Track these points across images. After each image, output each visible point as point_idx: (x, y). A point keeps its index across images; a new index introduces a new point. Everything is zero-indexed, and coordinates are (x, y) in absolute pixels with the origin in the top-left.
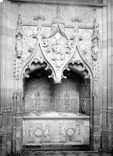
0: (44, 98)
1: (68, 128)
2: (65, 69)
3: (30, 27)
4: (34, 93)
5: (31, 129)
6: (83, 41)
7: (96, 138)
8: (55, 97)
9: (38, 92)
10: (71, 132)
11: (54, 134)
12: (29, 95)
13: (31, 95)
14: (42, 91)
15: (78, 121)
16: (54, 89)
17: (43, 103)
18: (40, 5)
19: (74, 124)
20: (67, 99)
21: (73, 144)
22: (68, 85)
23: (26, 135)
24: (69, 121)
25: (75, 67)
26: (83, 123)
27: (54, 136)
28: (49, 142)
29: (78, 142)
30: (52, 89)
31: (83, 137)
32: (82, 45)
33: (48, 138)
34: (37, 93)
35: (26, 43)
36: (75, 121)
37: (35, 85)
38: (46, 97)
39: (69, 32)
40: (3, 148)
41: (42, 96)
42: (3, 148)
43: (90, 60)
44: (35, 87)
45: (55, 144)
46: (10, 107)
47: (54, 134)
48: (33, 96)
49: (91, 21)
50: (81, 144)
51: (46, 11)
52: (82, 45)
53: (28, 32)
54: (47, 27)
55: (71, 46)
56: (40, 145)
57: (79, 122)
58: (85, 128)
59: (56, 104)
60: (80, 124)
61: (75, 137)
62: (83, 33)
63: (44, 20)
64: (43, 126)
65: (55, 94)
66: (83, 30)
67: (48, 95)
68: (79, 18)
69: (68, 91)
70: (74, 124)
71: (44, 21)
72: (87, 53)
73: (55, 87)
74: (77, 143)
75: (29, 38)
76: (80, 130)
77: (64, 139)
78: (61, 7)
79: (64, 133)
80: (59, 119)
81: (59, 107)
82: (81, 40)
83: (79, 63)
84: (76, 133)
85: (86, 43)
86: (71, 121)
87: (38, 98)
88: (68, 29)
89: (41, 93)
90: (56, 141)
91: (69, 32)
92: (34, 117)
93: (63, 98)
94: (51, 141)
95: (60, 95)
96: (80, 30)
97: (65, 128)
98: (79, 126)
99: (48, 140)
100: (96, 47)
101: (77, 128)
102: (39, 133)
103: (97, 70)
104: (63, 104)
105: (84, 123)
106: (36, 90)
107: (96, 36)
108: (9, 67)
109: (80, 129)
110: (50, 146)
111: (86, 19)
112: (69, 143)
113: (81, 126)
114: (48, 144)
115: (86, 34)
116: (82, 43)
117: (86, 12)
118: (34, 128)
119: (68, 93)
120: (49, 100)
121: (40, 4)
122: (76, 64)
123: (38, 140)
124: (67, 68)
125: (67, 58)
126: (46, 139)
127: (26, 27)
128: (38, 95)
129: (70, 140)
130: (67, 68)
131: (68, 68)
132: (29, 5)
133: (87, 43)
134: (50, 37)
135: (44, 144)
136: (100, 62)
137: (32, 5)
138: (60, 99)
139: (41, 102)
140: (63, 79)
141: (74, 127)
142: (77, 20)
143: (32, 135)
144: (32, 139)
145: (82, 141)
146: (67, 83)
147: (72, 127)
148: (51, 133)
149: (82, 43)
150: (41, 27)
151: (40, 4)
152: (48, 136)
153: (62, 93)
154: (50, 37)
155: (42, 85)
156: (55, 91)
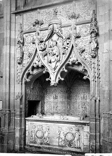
0: (62, 100)
1: (67, 132)
2: (61, 70)
3: (31, 33)
4: (52, 96)
5: (33, 130)
6: (81, 38)
7: (93, 147)
8: (72, 100)
9: (56, 95)
10: (69, 137)
11: (53, 137)
12: (48, 98)
13: (50, 98)
14: (59, 94)
15: (78, 126)
16: (71, 92)
17: (60, 107)
18: (38, 10)
19: (73, 128)
20: (84, 102)
21: (72, 150)
22: (85, 88)
23: (29, 136)
24: (69, 125)
25: (76, 68)
26: (83, 129)
27: (53, 139)
28: (49, 144)
29: (78, 148)
30: (68, 92)
31: (83, 144)
32: (81, 43)
33: (48, 140)
34: (55, 96)
35: (27, 49)
36: (74, 125)
37: (53, 88)
38: (63, 100)
39: (67, 32)
40: (5, 145)
41: (60, 99)
42: (5, 145)
43: (90, 58)
44: (53, 90)
45: (54, 147)
46: (14, 108)
47: (53, 137)
48: (52, 99)
49: (90, 14)
50: (80, 151)
51: (44, 15)
52: (81, 43)
53: (28, 38)
54: (45, 31)
55: (67, 45)
56: (41, 146)
57: (79, 127)
58: (85, 134)
59: (72, 107)
60: (80, 129)
61: (75, 143)
62: (82, 29)
63: (42, 24)
64: (44, 128)
65: (72, 97)
66: (81, 26)
67: (65, 98)
68: (77, 14)
69: (85, 93)
70: (73, 128)
71: (42, 25)
72: (86, 51)
73: (71, 90)
74: (76, 149)
75: (29, 45)
76: (79, 135)
77: (62, 143)
78: (59, 7)
79: (62, 136)
80: (57, 122)
81: (76, 110)
82: (78, 37)
83: (76, 63)
84: (76, 139)
85: (85, 40)
86: (71, 125)
87: (55, 101)
88: (65, 28)
89: (58, 96)
90: (55, 144)
91: (67, 32)
92: (37, 119)
93: (80, 100)
94: (50, 144)
95: (77, 97)
96: (78, 27)
97: (64, 132)
98: (78, 131)
99: (48, 143)
100: (93, 42)
101: (76, 134)
102: (39, 134)
103: (96, 69)
104: (80, 107)
105: (84, 128)
106: (54, 93)
107: (94, 29)
108: (13, 73)
109: (79, 134)
110: (49, 148)
111: (85, 13)
112: (68, 148)
113: (81, 132)
114: (47, 146)
115: (83, 30)
116: (80, 41)
117: (85, 5)
118: (36, 129)
119: (85, 96)
120: (66, 103)
121: (38, 9)
122: (74, 64)
123: (39, 141)
124: (64, 70)
125: (64, 59)
126: (46, 142)
127: (27, 34)
128: (56, 98)
129: (70, 145)
130: (64, 70)
131: (66, 69)
132: (30, 13)
133: (87, 40)
134: (47, 40)
135: (44, 146)
136: (101, 59)
137: (32, 13)
138: (76, 101)
139: (59, 105)
140: (60, 81)
141: (74, 132)
142: (73, 17)
143: (33, 136)
144: (34, 140)
145: (82, 148)
146: (84, 85)
147: (71, 132)
148: (50, 135)
149: (80, 41)
150: (39, 32)
151: (38, 9)
152: (47, 139)
153: (79, 95)
154: (47, 40)
155: (59, 88)
156: (72, 94)
